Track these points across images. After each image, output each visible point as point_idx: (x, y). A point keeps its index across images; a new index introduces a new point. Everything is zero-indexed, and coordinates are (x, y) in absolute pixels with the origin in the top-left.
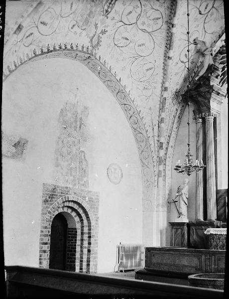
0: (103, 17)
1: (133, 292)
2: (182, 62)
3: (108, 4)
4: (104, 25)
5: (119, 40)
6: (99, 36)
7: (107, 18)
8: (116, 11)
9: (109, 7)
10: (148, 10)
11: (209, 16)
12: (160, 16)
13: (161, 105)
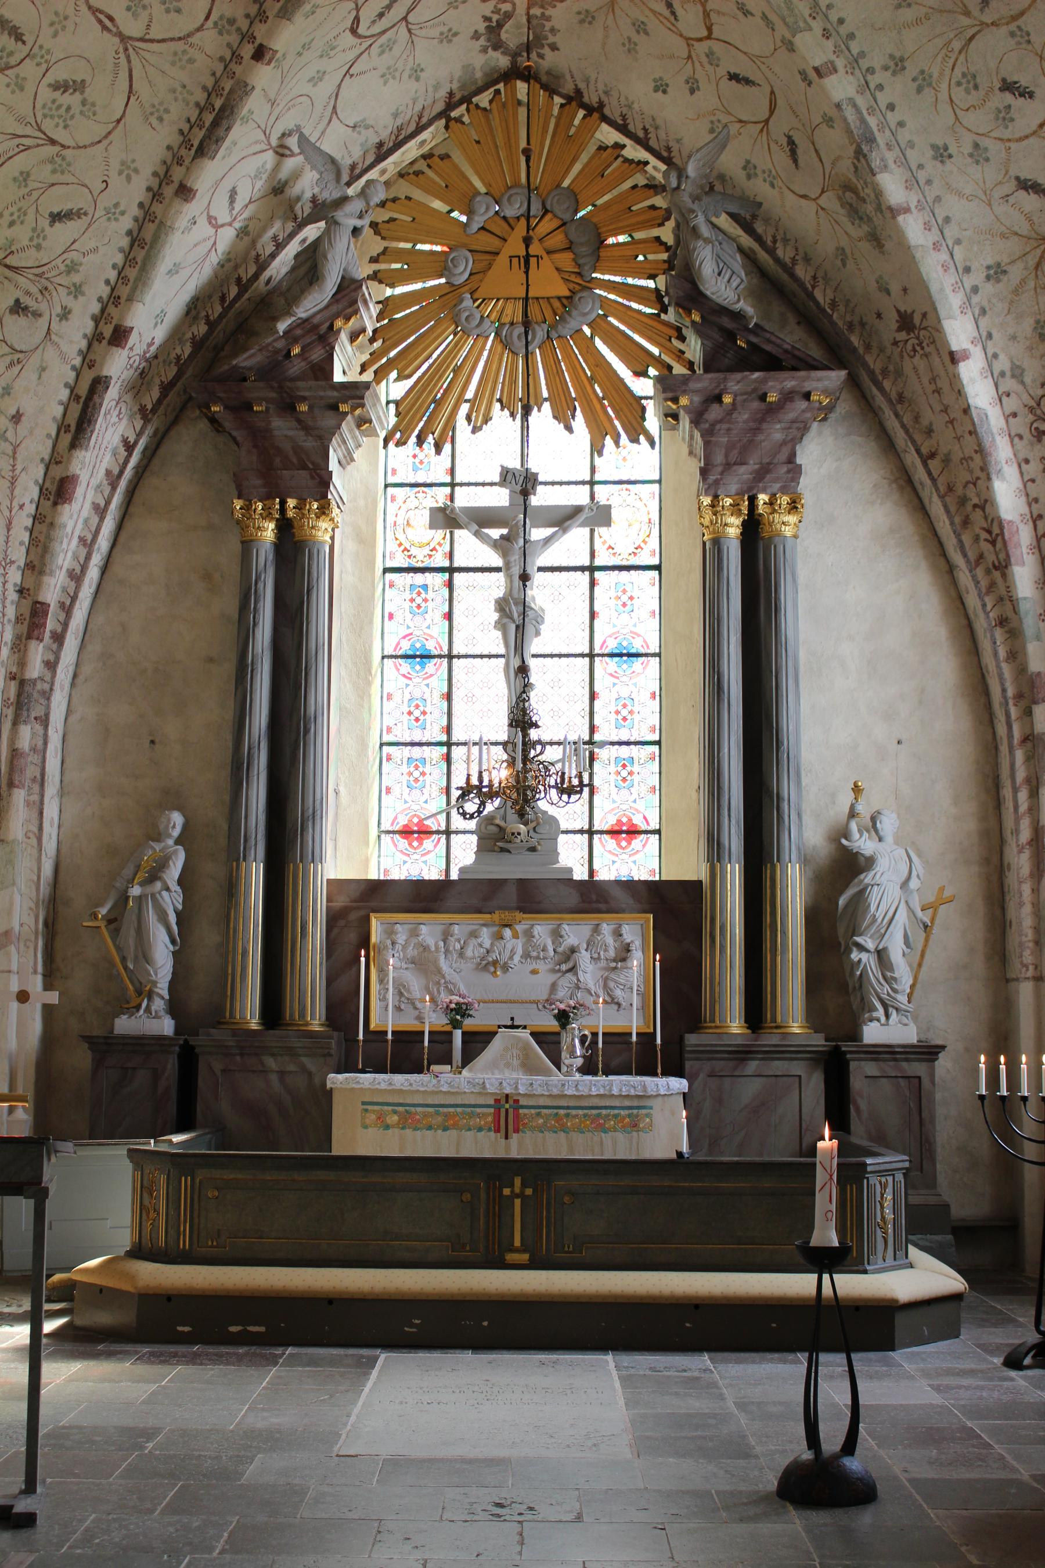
2: (211, 219)
11: (375, 49)
13: (76, 409)
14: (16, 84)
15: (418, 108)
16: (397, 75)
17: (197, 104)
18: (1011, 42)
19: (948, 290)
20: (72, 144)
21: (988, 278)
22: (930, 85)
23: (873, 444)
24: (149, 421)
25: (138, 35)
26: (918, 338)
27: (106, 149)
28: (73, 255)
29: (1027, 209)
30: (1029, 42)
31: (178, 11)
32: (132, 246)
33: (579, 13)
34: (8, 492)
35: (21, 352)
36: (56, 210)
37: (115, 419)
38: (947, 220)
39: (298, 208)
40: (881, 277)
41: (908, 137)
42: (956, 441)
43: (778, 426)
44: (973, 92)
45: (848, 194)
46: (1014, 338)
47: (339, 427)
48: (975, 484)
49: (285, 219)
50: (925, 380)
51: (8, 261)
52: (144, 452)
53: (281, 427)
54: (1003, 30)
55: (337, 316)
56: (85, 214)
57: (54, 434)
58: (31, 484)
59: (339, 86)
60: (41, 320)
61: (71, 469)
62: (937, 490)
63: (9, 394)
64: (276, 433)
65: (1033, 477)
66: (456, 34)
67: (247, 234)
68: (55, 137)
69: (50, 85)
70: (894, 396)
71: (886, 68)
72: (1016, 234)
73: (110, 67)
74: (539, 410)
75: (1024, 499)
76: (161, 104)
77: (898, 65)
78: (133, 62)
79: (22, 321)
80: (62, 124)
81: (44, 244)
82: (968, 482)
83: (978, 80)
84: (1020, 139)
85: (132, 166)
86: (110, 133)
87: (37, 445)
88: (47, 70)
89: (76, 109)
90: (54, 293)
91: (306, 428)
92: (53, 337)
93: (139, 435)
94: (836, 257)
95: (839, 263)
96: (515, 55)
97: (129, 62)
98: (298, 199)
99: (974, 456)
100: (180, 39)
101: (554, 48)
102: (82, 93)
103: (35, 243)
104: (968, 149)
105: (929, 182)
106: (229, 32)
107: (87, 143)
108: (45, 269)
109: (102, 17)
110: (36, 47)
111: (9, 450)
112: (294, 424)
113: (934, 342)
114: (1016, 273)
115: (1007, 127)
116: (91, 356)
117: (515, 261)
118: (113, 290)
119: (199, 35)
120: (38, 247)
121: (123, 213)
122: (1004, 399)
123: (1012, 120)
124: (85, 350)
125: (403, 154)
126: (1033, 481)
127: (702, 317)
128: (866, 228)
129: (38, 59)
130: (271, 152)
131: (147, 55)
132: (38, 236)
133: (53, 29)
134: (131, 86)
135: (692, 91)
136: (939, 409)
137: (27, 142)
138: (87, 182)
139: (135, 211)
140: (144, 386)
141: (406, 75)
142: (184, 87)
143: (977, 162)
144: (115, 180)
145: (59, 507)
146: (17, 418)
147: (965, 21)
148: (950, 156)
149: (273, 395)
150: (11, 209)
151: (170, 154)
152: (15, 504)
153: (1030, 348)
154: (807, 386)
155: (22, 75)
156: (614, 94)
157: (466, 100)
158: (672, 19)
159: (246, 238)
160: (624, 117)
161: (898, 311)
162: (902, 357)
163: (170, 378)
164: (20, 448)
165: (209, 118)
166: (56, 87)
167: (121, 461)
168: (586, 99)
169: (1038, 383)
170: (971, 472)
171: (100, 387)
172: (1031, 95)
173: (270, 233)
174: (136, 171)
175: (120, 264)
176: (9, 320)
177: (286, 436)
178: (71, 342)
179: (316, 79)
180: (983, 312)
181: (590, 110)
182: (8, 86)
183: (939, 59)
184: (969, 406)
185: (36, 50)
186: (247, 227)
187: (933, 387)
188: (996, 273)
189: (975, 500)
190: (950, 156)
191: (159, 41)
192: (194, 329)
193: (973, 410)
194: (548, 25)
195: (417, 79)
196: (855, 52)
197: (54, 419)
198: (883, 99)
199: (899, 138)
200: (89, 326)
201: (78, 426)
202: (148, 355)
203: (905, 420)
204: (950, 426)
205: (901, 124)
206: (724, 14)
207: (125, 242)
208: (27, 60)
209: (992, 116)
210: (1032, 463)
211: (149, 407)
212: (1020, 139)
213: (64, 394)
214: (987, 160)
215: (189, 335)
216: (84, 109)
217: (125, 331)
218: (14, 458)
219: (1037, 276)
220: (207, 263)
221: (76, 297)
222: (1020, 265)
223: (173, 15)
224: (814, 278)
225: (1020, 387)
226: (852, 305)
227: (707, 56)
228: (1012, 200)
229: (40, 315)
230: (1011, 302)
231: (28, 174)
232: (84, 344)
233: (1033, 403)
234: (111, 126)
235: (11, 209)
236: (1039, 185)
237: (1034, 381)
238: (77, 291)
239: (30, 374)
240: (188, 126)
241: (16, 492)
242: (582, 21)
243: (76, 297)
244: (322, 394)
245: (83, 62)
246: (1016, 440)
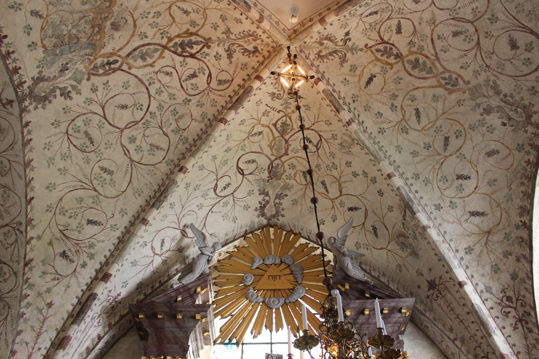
0: (84, 70)
1: (261, 321)
3: (106, 60)
4: (75, 83)
5: (79, 132)
6: (53, 91)
7: (88, 79)
8: (108, 82)
9: (103, 66)
10: (153, 125)
12: (165, 146)
13: (79, 307)
14: (86, 160)
15: (234, 234)
16: (228, 218)
17: (155, 191)
18: (458, 160)
19: (452, 258)
20: (103, 194)
21: (466, 253)
22: (429, 182)
23: (425, 342)
24: (112, 328)
25: (137, 161)
26: (438, 291)
27: (116, 202)
28: (93, 240)
29: (476, 223)
30: (465, 158)
31: (153, 155)
32: (118, 244)
33: (292, 201)
34: (35, 339)
35: (60, 275)
36: (91, 219)
37: (96, 324)
38: (445, 232)
39: (187, 261)
40: (418, 269)
41: (425, 202)
42: (466, 330)
43: (389, 325)
44: (446, 183)
45: (401, 238)
46: (483, 275)
47: (195, 327)
48: (480, 347)
49: (181, 263)
50: (445, 308)
51: (65, 232)
52: (107, 343)
53: (169, 326)
54: (454, 156)
55: (198, 285)
56: (102, 225)
57: (65, 318)
58: (48, 339)
59: (207, 214)
60: (73, 264)
61: (68, 333)
62: (463, 353)
63: (49, 292)
64: (166, 329)
65: (509, 334)
66: (249, 207)
67: (166, 264)
68: (97, 189)
69: (99, 167)
70: (432, 318)
71: (413, 178)
72: (474, 234)
73: (124, 170)
74: (282, 329)
75: (508, 345)
76: (141, 189)
77: (417, 177)
78: (133, 171)
79: (64, 261)
80: (101, 185)
81: (82, 232)
82: (476, 348)
83: (447, 178)
84: (468, 196)
85: (125, 211)
86: (119, 195)
87: (56, 321)
88: (100, 161)
89: (108, 181)
90: (82, 255)
91: (180, 327)
92: (77, 274)
93: (105, 334)
94: (397, 269)
95: (398, 271)
96: (269, 220)
97: (132, 170)
98: (188, 257)
99: (477, 333)
100: (152, 165)
101: (283, 216)
102: (112, 176)
103: (78, 229)
104: (448, 204)
105: (435, 219)
106: (171, 165)
107: (109, 196)
108: (80, 242)
109: (125, 149)
110: (98, 149)
111: (42, 319)
112: (175, 325)
113: (447, 288)
114: (477, 249)
115: (462, 193)
116: (91, 286)
117: (271, 277)
118: (107, 260)
119: (159, 164)
120: (79, 232)
121: (117, 229)
122: (486, 302)
123: (464, 189)
124: (89, 284)
125: (228, 248)
126: (510, 336)
127: (350, 287)
128: (409, 250)
129: (97, 155)
130: (179, 231)
131: (139, 169)
132: (80, 227)
133: (105, 146)
134: (131, 180)
135: (334, 221)
136: (454, 318)
137: (85, 186)
138: (106, 212)
139: (122, 229)
140: (112, 315)
141: (231, 219)
142: (151, 183)
143: (453, 209)
144: (117, 215)
145: (58, 351)
146: (50, 305)
147: (439, 157)
148: (442, 208)
149: (167, 310)
150: (72, 211)
151: (141, 209)
152: (37, 346)
153: (492, 278)
154: (400, 305)
155: (89, 157)
156: (305, 229)
157: (252, 232)
158: (327, 193)
159: (165, 266)
160: (309, 236)
161: (428, 281)
162: (431, 302)
163: (124, 313)
164: (47, 320)
165: (158, 195)
166: (102, 169)
167: (95, 343)
168: (294, 232)
169: (499, 292)
170: (476, 341)
171: (91, 298)
172: (469, 178)
173: (175, 268)
174: (126, 214)
175: (112, 250)
176: (58, 258)
177: (171, 331)
178: (84, 278)
179: (200, 207)
180: (467, 267)
181: (295, 234)
182: (83, 159)
183: (432, 173)
184: (473, 304)
185: (97, 150)
186: (166, 261)
187: (450, 308)
188: (469, 250)
189: (482, 354)
190: (442, 208)
191: (145, 165)
192: (139, 297)
193: (475, 306)
194: (281, 207)
195: (235, 222)
196: (401, 172)
197: (68, 311)
198: (413, 189)
199: (422, 203)
200: (93, 274)
201: (77, 315)
202: (117, 300)
203: (439, 326)
204: (461, 323)
205: (421, 198)
206: (347, 182)
207: (116, 241)
208: (93, 153)
209: (455, 190)
210: (506, 328)
211: (113, 323)
212: (468, 196)
213: (75, 301)
214: (456, 207)
215: (136, 299)
216: (111, 182)
217: (108, 275)
218: (43, 324)
219: (487, 248)
220: (148, 269)
221: (90, 259)
222: (478, 245)
223: (151, 156)
224: (388, 281)
225: (492, 296)
226: (406, 287)
227: (340, 204)
228: (469, 221)
229: (73, 262)
230: (478, 261)
231: (82, 199)
232: (89, 281)
233: (499, 301)
234: (120, 193)
235: (72, 211)
236: (479, 212)
237: (497, 291)
238: (91, 256)
239: (61, 288)
240: (149, 198)
241: (39, 341)
242: (293, 204)
243: (90, 259)
244: (189, 309)
245: (114, 164)
246: (496, 319)
